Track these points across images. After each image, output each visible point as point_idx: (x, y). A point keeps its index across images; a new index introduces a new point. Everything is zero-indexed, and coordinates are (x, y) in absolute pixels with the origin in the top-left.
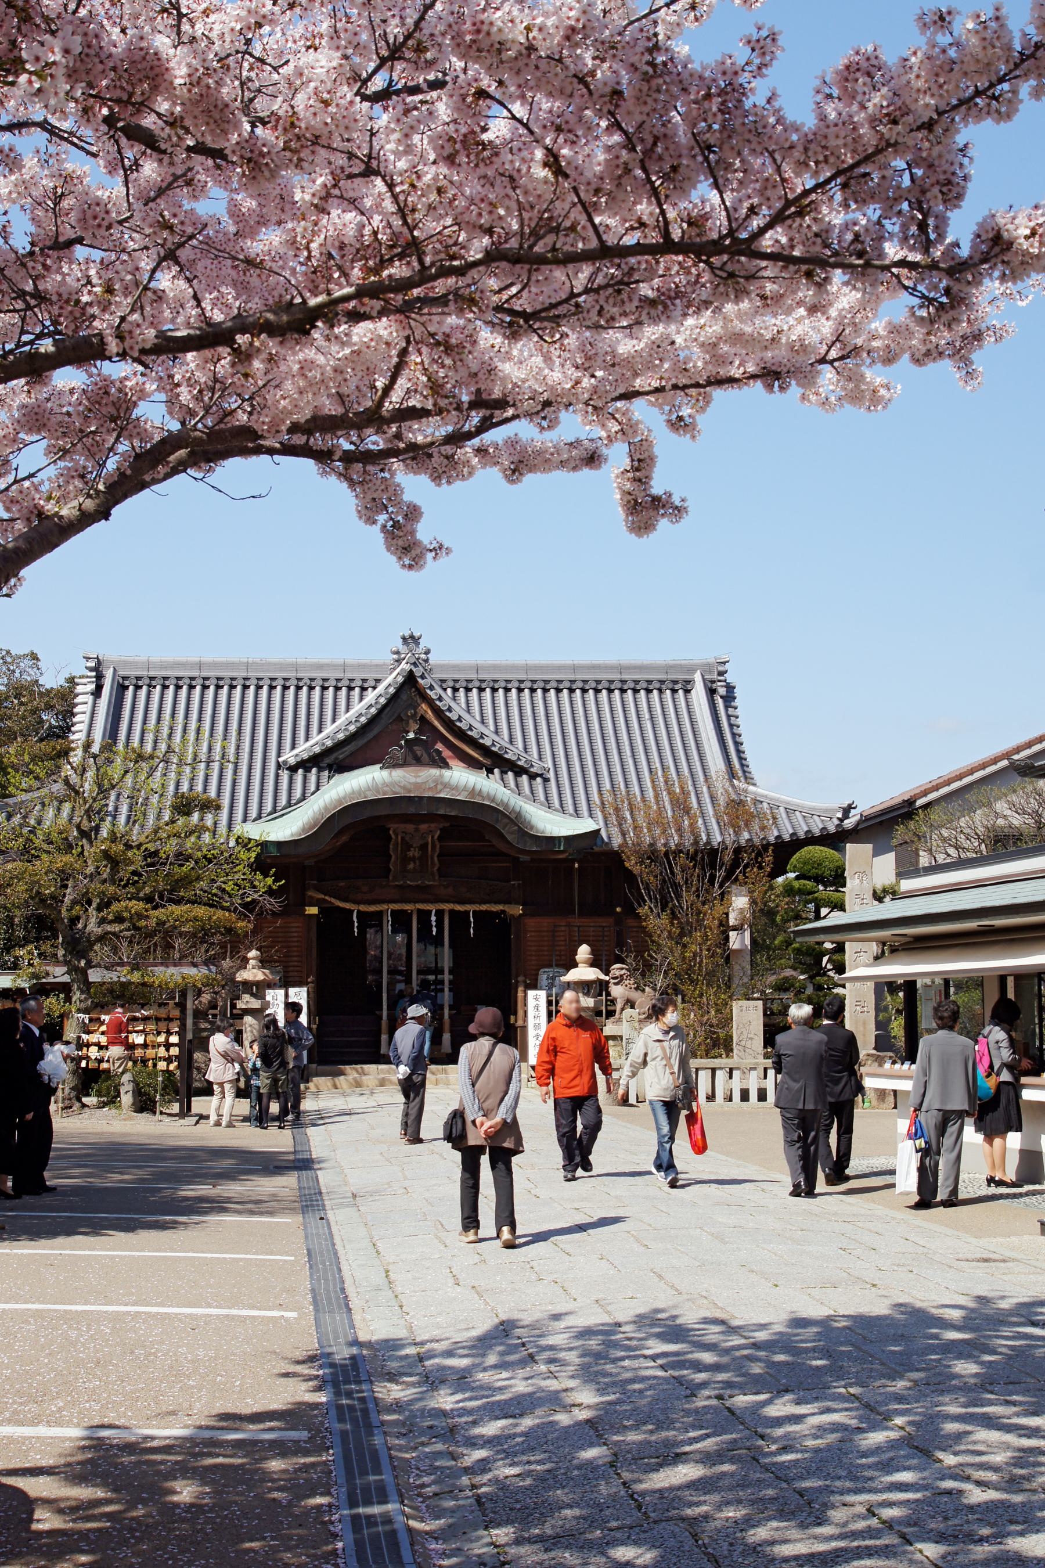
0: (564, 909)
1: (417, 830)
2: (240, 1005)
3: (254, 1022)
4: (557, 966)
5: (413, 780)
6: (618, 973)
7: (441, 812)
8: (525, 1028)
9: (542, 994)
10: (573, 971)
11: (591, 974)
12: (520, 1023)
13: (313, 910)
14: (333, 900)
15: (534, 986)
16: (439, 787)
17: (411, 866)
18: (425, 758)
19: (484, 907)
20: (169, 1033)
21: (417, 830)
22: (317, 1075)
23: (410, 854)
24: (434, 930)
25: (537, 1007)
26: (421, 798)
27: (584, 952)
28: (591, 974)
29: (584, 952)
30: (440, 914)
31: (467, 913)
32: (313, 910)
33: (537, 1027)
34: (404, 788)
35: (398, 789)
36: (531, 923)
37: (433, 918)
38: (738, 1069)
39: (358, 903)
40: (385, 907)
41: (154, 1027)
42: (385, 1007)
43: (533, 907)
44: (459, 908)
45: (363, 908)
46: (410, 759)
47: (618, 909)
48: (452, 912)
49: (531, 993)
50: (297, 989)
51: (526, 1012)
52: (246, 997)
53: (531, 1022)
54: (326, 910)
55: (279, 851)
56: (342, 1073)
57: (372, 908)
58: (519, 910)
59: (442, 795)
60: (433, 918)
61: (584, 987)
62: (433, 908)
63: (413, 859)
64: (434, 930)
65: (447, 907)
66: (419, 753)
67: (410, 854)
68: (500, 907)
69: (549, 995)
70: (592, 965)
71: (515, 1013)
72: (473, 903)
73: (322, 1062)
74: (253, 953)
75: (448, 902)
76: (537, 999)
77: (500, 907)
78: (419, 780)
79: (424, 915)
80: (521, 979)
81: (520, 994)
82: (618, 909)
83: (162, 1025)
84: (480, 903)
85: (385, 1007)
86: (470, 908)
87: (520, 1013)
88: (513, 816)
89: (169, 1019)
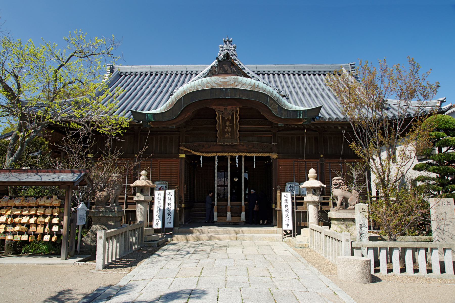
0: (298, 156)
1: (225, 109)
2: (135, 198)
3: (142, 207)
4: (296, 181)
5: (222, 80)
6: (338, 182)
7: (238, 97)
8: (280, 211)
9: (289, 194)
10: (306, 182)
11: (318, 184)
12: (278, 208)
13: (183, 156)
14: (192, 151)
15: (284, 191)
16: (236, 84)
17: (227, 136)
18: (229, 71)
19: (260, 155)
20: (52, 216)
21: (225, 109)
22: (178, 233)
23: (226, 130)
24: (237, 165)
25: (286, 201)
26: (226, 89)
27: (312, 172)
28: (318, 184)
29: (312, 172)
30: (240, 158)
31: (252, 157)
32: (183, 156)
33: (287, 210)
34: (217, 84)
35: (214, 85)
36: (282, 162)
37: (237, 160)
38: (450, 249)
39: (203, 152)
40: (215, 154)
41: (42, 212)
42: (216, 200)
43: (283, 155)
44: (248, 155)
45: (205, 155)
46: (221, 72)
47: (322, 156)
48: (246, 157)
49: (283, 194)
50: (170, 191)
51: (281, 203)
52: (138, 194)
53: (284, 208)
54: (190, 157)
55: (154, 119)
56: (191, 232)
57: (209, 155)
58: (275, 156)
59: (238, 87)
60: (237, 160)
61: (314, 190)
62: (237, 155)
63: (228, 132)
64: (237, 165)
65: (243, 154)
66: (226, 69)
67: (226, 130)
68: (268, 155)
69: (292, 195)
70: (316, 179)
71: (276, 204)
72: (255, 153)
73: (180, 226)
74: (143, 172)
75: (244, 152)
76: (286, 197)
77: (268, 155)
78: (226, 80)
79: (233, 159)
80: (278, 187)
81: (278, 194)
82: (322, 156)
83: (48, 212)
84: (258, 153)
85: (216, 200)
86: (254, 155)
87: (278, 203)
88: (276, 99)
89: (53, 207)
